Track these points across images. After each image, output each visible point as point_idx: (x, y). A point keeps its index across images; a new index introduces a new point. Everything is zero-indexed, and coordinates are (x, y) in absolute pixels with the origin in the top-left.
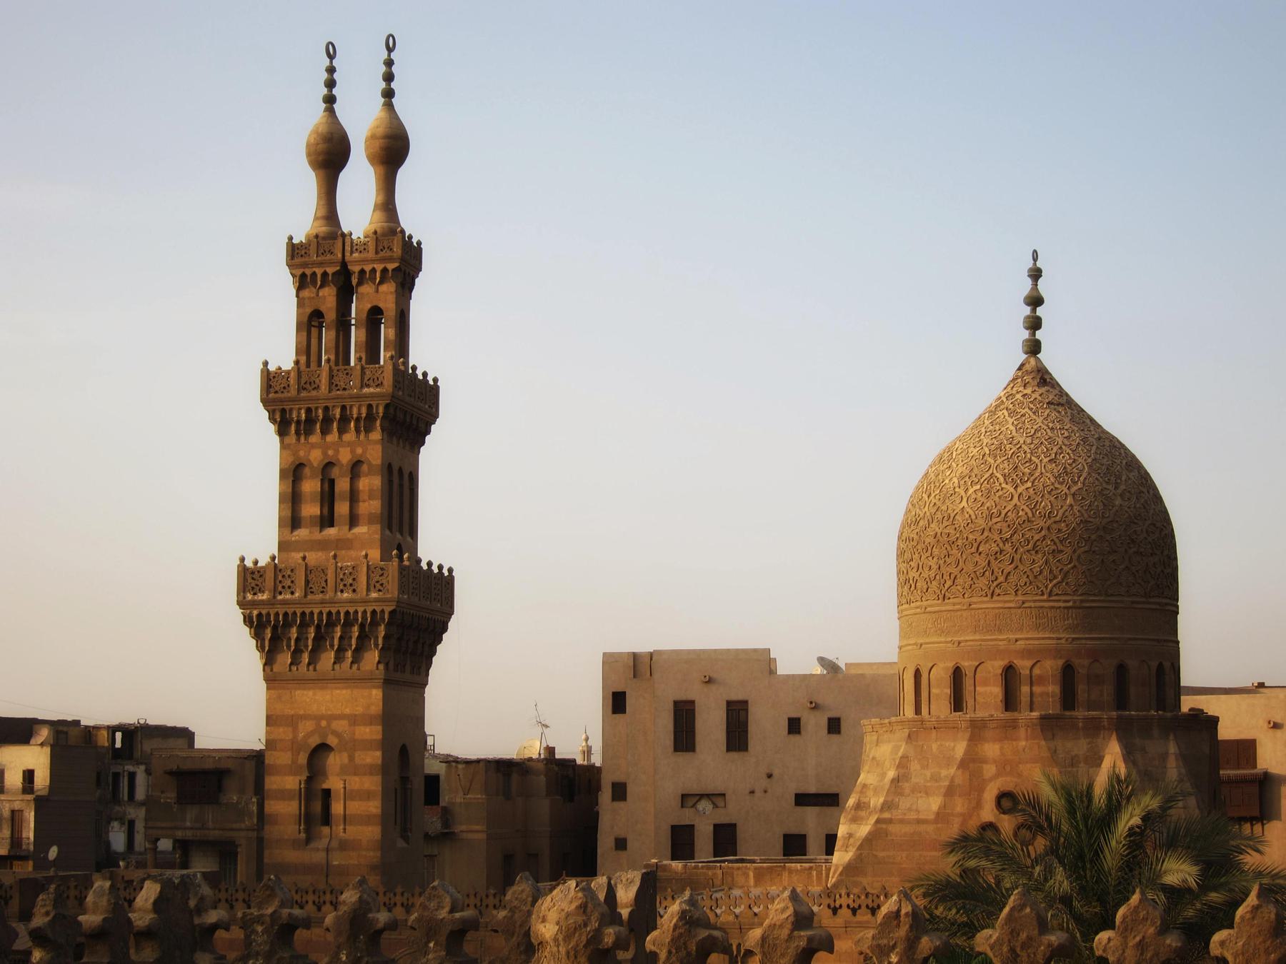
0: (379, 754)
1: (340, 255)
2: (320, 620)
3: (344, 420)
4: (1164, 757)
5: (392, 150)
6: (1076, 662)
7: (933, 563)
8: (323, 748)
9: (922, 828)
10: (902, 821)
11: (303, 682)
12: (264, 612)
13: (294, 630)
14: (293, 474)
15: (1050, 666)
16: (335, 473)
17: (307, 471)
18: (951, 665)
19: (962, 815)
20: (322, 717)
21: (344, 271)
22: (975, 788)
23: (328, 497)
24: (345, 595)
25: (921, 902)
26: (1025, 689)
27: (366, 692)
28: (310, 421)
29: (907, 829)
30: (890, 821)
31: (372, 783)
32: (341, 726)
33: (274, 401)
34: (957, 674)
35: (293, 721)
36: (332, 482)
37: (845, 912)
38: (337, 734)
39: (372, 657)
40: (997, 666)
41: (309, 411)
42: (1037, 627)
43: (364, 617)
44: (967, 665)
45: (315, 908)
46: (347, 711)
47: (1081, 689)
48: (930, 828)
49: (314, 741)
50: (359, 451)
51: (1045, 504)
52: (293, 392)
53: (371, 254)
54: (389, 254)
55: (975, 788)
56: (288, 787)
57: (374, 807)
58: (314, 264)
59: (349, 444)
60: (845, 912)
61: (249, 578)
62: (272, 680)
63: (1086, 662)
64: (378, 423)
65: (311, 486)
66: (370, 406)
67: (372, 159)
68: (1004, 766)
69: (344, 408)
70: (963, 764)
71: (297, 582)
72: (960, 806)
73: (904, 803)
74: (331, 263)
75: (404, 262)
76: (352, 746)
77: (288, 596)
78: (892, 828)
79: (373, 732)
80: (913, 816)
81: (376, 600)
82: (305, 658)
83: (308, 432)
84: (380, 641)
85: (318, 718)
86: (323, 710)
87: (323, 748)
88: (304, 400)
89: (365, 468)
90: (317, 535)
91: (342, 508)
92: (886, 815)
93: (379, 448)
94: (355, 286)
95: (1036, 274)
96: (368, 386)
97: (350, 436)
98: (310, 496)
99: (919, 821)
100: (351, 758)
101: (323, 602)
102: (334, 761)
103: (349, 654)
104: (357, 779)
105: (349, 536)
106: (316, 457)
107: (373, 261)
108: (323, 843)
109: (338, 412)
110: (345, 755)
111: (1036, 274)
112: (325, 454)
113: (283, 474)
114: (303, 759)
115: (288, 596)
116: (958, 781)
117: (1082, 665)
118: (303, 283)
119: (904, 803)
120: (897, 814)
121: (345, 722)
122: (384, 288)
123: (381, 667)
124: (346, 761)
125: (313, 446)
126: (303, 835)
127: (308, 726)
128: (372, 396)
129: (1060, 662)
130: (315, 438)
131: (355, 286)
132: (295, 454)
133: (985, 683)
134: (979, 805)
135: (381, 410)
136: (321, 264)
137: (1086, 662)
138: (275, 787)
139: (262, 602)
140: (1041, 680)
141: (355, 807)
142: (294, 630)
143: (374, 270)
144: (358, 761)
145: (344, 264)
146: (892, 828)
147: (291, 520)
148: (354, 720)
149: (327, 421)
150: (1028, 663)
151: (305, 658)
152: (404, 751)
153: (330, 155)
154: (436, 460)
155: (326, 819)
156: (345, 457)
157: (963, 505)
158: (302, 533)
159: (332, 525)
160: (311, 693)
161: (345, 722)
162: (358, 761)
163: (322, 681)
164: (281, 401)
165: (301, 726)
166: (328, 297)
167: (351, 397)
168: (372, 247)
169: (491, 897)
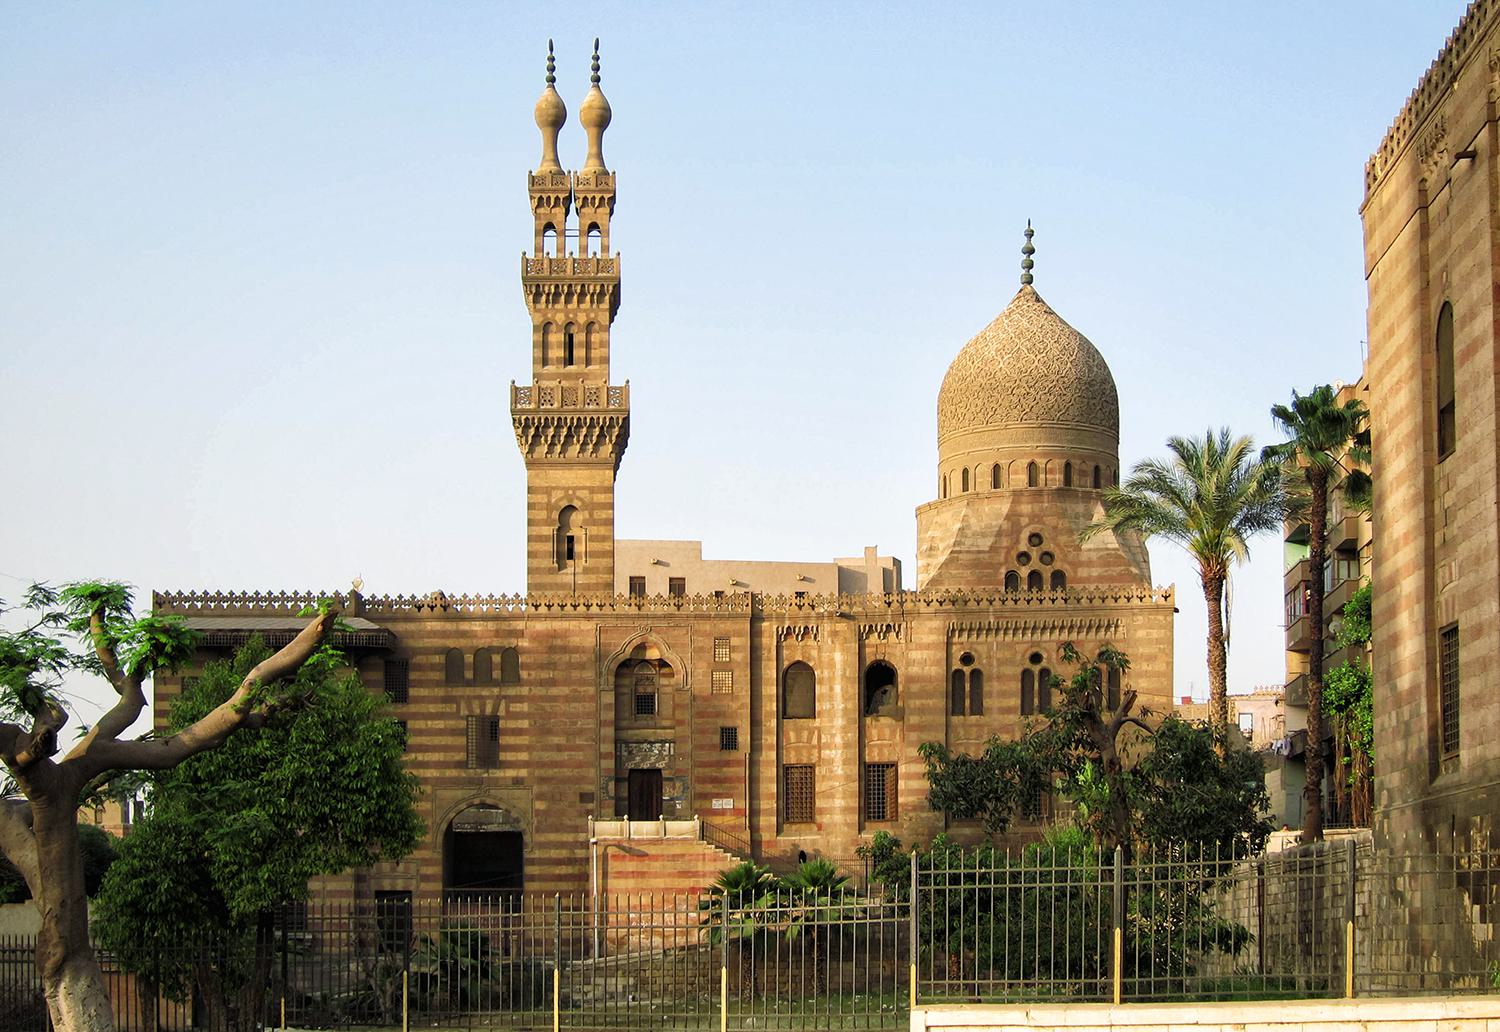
2: (572, 423)
3: (582, 295)
5: (602, 120)
6: (1072, 461)
7: (980, 403)
8: (571, 508)
9: (981, 555)
10: (967, 552)
11: (553, 465)
12: (530, 417)
13: (552, 429)
14: (544, 328)
15: (1058, 463)
16: (574, 329)
17: (553, 328)
18: (992, 463)
19: (1007, 547)
22: (1015, 530)
23: (569, 345)
24: (591, 407)
25: (326, 949)
26: (1042, 476)
27: (601, 472)
28: (557, 295)
30: (960, 552)
34: (997, 468)
35: (548, 491)
36: (571, 337)
37: (935, 604)
38: (581, 499)
40: (1024, 462)
41: (557, 286)
42: (1049, 439)
43: (604, 422)
44: (1003, 463)
45: (585, 609)
46: (588, 485)
47: (1075, 478)
48: (986, 556)
49: (564, 504)
50: (592, 315)
51: (1056, 366)
52: (546, 273)
53: (593, 186)
54: (606, 187)
55: (1015, 530)
58: (549, 190)
59: (585, 311)
60: (935, 604)
62: (531, 464)
63: (1078, 462)
64: (607, 298)
65: (556, 337)
66: (602, 286)
67: (586, 125)
68: (1035, 518)
69: (583, 286)
70: (1008, 517)
71: (555, 397)
72: (1005, 542)
77: (549, 407)
81: (613, 410)
82: (558, 448)
83: (555, 301)
84: (614, 438)
85: (566, 489)
87: (571, 508)
88: (554, 279)
89: (596, 326)
90: (562, 370)
91: (579, 353)
92: (957, 549)
95: (1030, 234)
96: (602, 272)
97: (586, 305)
99: (979, 552)
100: (591, 515)
101: (575, 411)
102: (576, 518)
103: (591, 446)
105: (586, 371)
106: (560, 318)
107: (594, 191)
108: (570, 570)
109: (579, 288)
110: (586, 513)
111: (1030, 234)
112: (567, 316)
113: (536, 329)
114: (555, 515)
115: (549, 407)
116: (1005, 527)
117: (1076, 463)
121: (586, 492)
122: (600, 210)
123: (613, 455)
124: (587, 516)
125: (558, 311)
126: (556, 565)
127: (559, 494)
128: (605, 279)
129: (1064, 461)
130: (560, 305)
132: (544, 315)
133: (1016, 473)
134: (1017, 542)
135: (611, 288)
136: (554, 191)
137: (1078, 462)
139: (529, 411)
140: (1052, 471)
142: (552, 429)
143: (594, 198)
144: (595, 516)
149: (570, 295)
150: (1045, 461)
151: (558, 448)
155: (571, 555)
156: (582, 319)
157: (1003, 366)
158: (550, 369)
159: (571, 363)
161: (586, 492)
162: (595, 516)
163: (569, 465)
164: (537, 279)
165: (554, 493)
167: (590, 279)
168: (593, 181)
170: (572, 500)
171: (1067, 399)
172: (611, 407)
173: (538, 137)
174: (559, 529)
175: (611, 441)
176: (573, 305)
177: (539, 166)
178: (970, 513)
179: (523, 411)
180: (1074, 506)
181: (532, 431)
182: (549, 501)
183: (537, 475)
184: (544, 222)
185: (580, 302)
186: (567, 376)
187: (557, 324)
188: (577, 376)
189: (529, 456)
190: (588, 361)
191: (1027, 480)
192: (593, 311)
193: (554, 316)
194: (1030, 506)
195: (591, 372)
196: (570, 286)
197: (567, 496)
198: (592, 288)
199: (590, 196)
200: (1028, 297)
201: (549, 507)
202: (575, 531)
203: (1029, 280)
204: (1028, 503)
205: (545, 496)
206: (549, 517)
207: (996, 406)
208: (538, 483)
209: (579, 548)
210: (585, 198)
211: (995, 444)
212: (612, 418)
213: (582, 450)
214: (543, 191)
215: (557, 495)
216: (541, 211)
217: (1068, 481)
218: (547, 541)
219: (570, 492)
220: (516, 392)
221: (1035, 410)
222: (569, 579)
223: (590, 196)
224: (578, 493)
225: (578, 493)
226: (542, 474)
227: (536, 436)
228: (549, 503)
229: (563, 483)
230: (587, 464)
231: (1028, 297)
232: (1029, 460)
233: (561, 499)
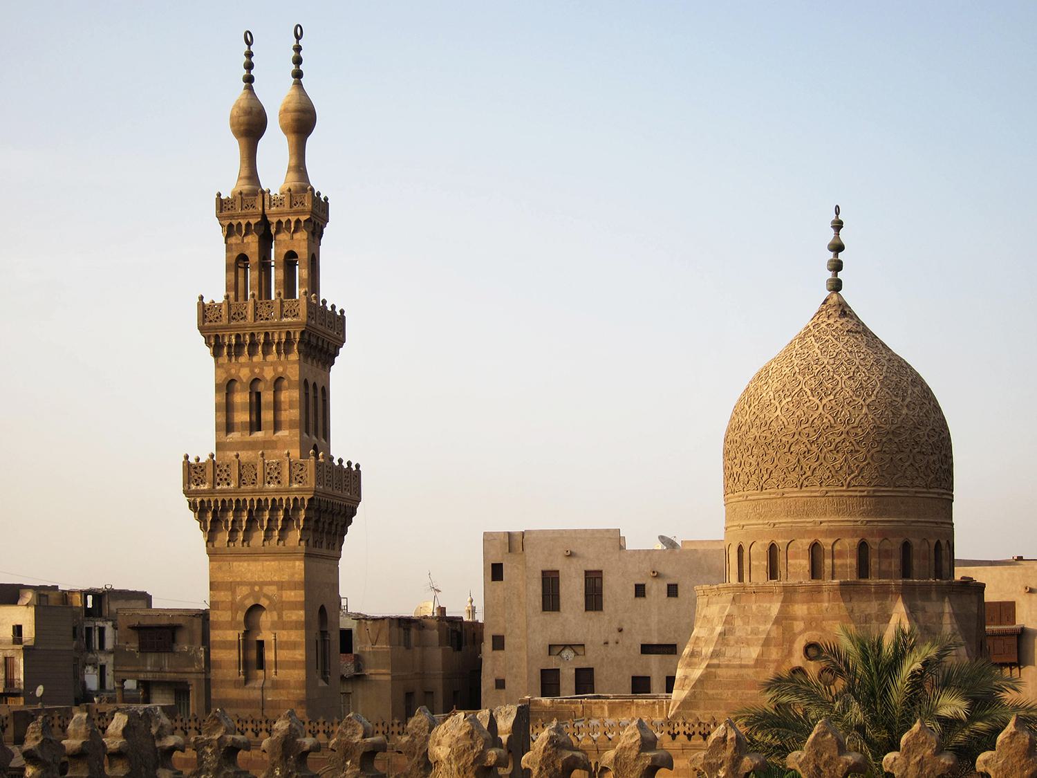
0: (302, 613)
1: (260, 209)
2: (252, 506)
4: (940, 615)
5: (302, 123)
6: (869, 540)
7: (753, 460)
9: (744, 671)
10: (727, 666)
11: (239, 555)
13: (231, 514)
14: (227, 387)
15: (850, 543)
17: (238, 385)
18: (767, 542)
20: (255, 583)
21: (265, 222)
23: (256, 406)
24: (272, 486)
26: (828, 562)
28: (239, 345)
29: (733, 672)
30: (718, 666)
31: (298, 636)
32: (271, 590)
33: (209, 328)
35: (232, 587)
36: (259, 395)
39: (295, 536)
41: (238, 336)
44: (781, 542)
45: (253, 734)
46: (276, 579)
48: (751, 672)
49: (250, 602)
50: (280, 369)
52: (224, 321)
53: (286, 208)
54: (301, 207)
55: (788, 640)
56: (229, 639)
57: (300, 654)
58: (239, 216)
59: (272, 364)
61: (192, 472)
62: (212, 554)
63: (877, 540)
65: (241, 397)
67: (285, 129)
68: (811, 623)
71: (232, 475)
72: (775, 654)
73: (730, 652)
74: (253, 215)
75: (316, 217)
76: (280, 606)
77: (225, 487)
78: (719, 671)
79: (298, 595)
80: (737, 662)
81: (297, 490)
82: (241, 536)
84: (301, 523)
85: (252, 584)
86: (256, 578)
87: (256, 608)
88: (285, 325)
89: (285, 383)
91: (267, 416)
92: (715, 661)
93: (297, 366)
95: (838, 225)
96: (287, 316)
97: (272, 357)
98: (241, 407)
99: (741, 666)
100: (280, 616)
101: (253, 491)
102: (266, 619)
103: (276, 533)
104: (285, 632)
105: (274, 438)
107: (288, 214)
108: (258, 683)
109: (262, 337)
110: (275, 613)
111: (838, 225)
112: (252, 371)
114: (241, 617)
115: (225, 487)
116: (773, 634)
118: (230, 231)
119: (730, 652)
120: (723, 661)
121: (274, 588)
122: (297, 236)
123: (303, 543)
124: (276, 618)
125: (242, 365)
126: (242, 677)
127: (243, 591)
128: (290, 324)
129: (857, 540)
130: (244, 359)
131: (273, 236)
132: (228, 371)
133: (795, 556)
134: (790, 653)
135: (298, 336)
136: (245, 216)
138: (218, 639)
139: (204, 492)
140: (841, 554)
141: (284, 655)
142: (231, 514)
143: (289, 221)
144: (285, 618)
145: (264, 216)
146: (719, 671)
147: (227, 426)
148: (281, 586)
150: (831, 541)
151: (241, 536)
152: (322, 610)
153: (251, 127)
154: (343, 377)
155: (261, 664)
156: (269, 374)
157: (778, 414)
158: (235, 436)
160: (245, 564)
163: (254, 555)
166: (252, 244)
167: (273, 325)
168: (287, 202)
169: (396, 726)
170: (259, 599)
171: (860, 456)
172: (295, 486)
173: (233, 148)
174: (246, 633)
175: (298, 526)
176: (258, 358)
177: (229, 183)
178: (736, 612)
179: (197, 493)
180: (863, 605)
181: (210, 516)
182: (234, 599)
183: (220, 568)
184: (236, 254)
185: (265, 353)
186: (252, 446)
187: (242, 382)
188: (267, 444)
189: (209, 544)
190: (277, 426)
191: (808, 567)
192: (281, 364)
193: (285, 370)
194: (805, 607)
195: (279, 439)
196: (252, 335)
197: (252, 594)
198: (276, 336)
199: (284, 220)
200: (831, 311)
201: (234, 607)
202: (266, 635)
203: (836, 286)
204: (803, 602)
205: (230, 593)
206: (233, 619)
207: (771, 467)
208: (221, 577)
209: (269, 655)
210: (279, 222)
211: (772, 516)
212: (259, 500)
213: (267, 537)
214: (232, 217)
215: (243, 591)
216: (233, 240)
217: (863, 569)
218: (231, 648)
219: (257, 588)
220: (192, 472)
221: (818, 473)
222: (256, 694)
223: (284, 220)
224: (266, 589)
225: (266, 589)
226: (225, 566)
227: (215, 521)
228: (233, 603)
229: (248, 577)
230: (275, 555)
231: (831, 311)
232: (811, 540)
233: (246, 597)
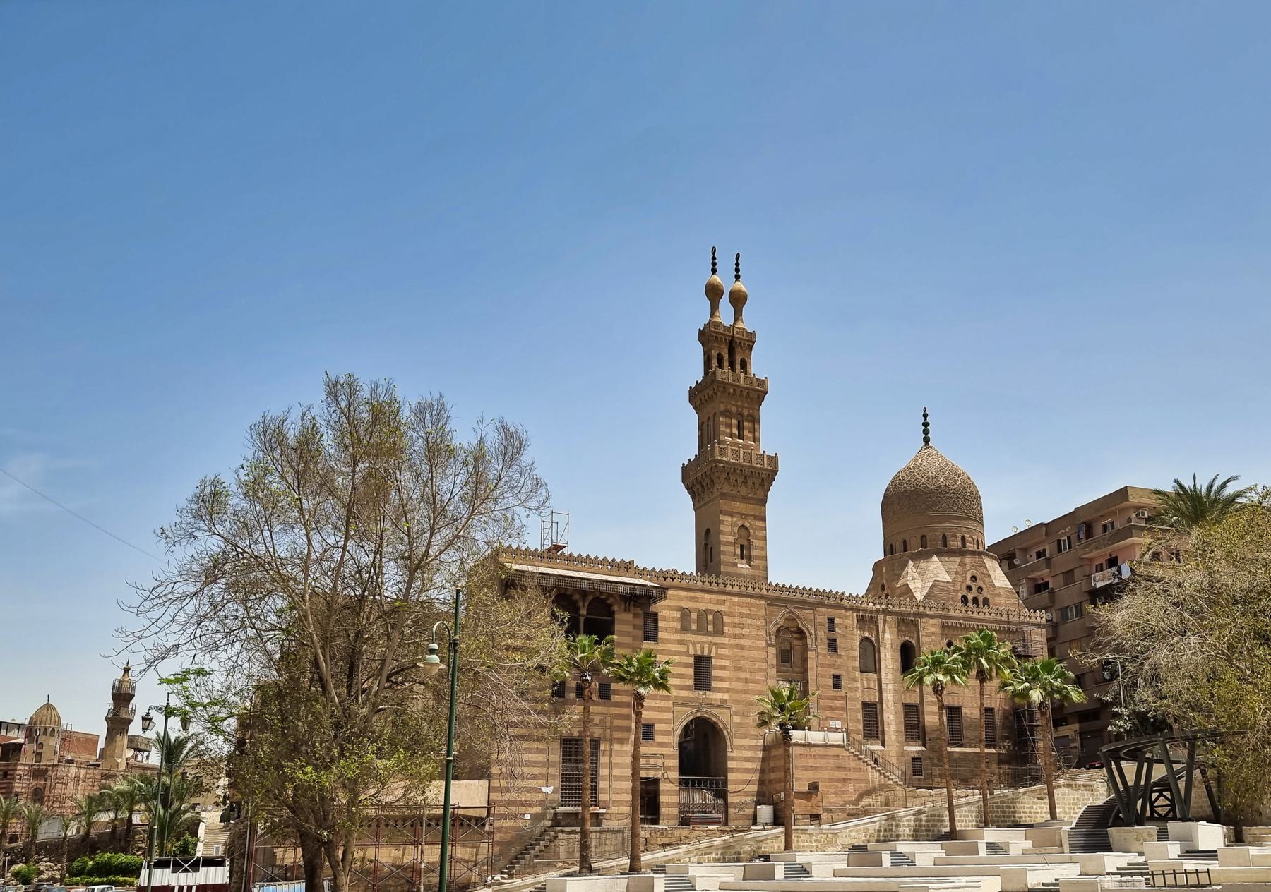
5: (738, 300)
94: (725, 347)
131: (725, 347)
152: (708, 531)
